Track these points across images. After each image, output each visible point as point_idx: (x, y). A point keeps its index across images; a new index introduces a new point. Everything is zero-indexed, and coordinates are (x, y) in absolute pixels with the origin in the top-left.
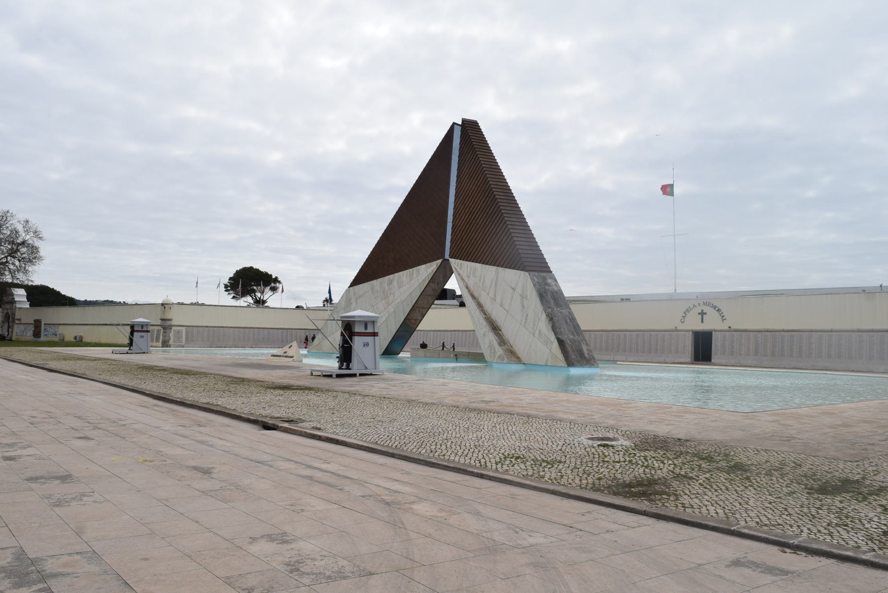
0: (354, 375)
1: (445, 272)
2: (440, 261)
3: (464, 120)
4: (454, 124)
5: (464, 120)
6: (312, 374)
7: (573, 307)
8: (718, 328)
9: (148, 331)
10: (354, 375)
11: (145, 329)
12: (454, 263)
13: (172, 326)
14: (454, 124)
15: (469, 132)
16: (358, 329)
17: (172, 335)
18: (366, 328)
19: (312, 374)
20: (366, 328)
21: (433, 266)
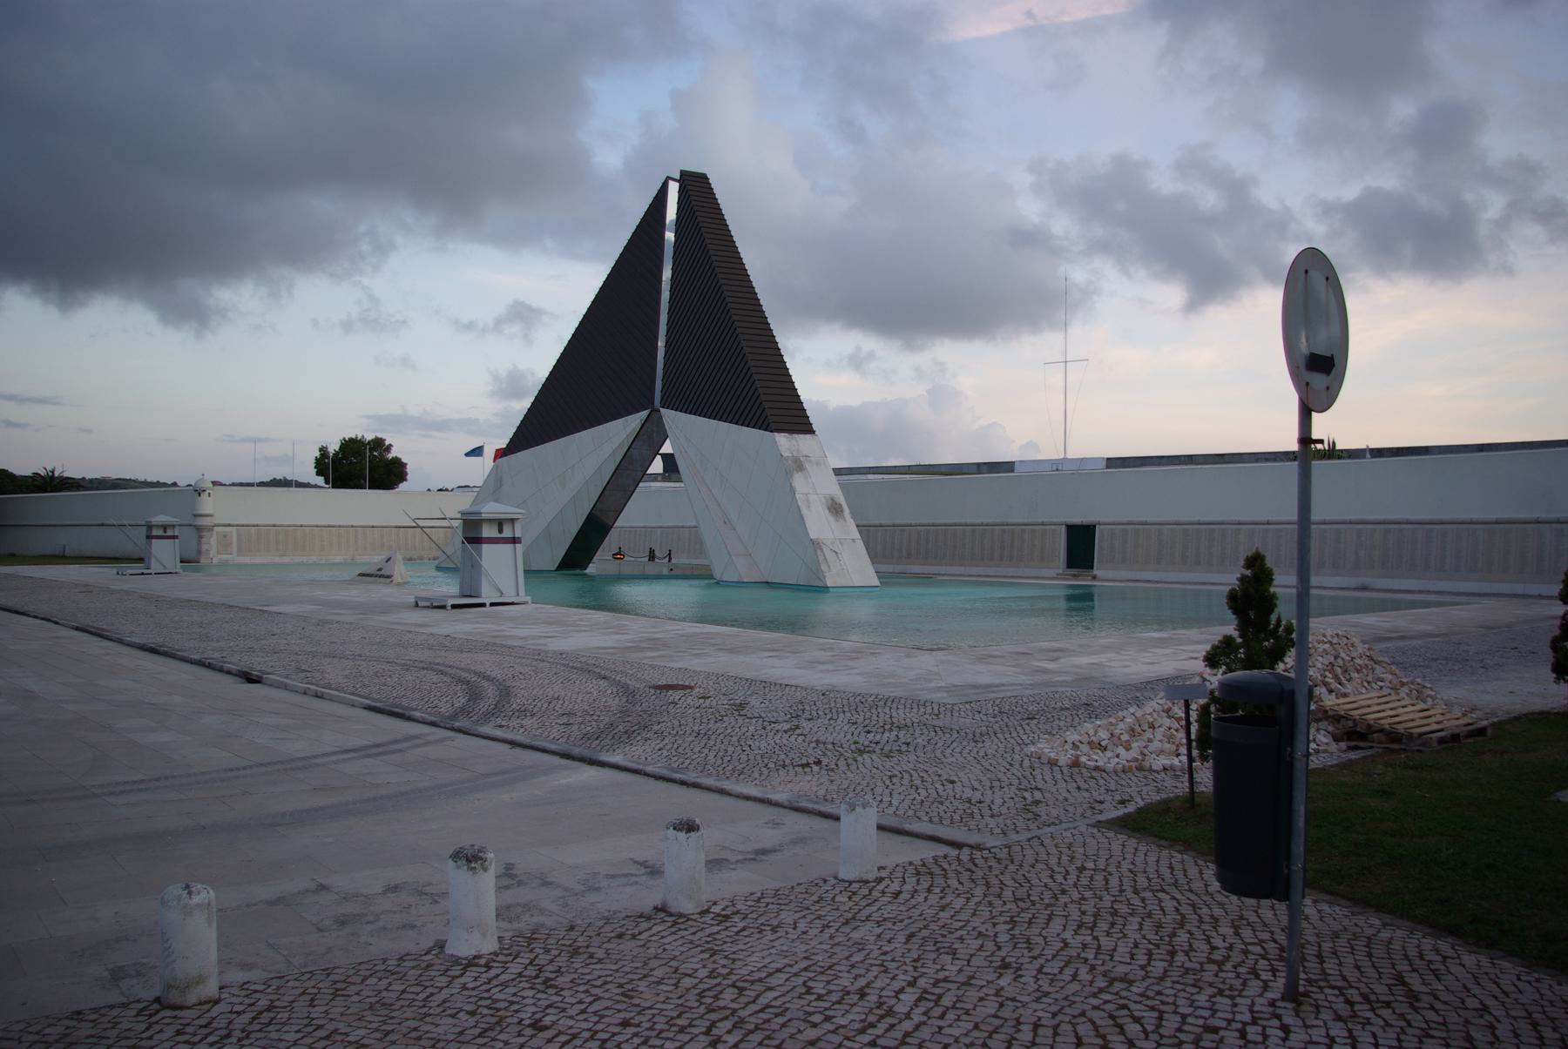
0: (483, 605)
1: (651, 436)
2: (644, 414)
3: (683, 173)
4: (668, 178)
5: (683, 173)
6: (417, 605)
7: (207, 505)
8: (1103, 519)
9: (174, 537)
10: (483, 605)
11: (169, 533)
12: (673, 419)
13: (210, 529)
14: (668, 178)
15: (696, 187)
16: (488, 532)
17: (213, 541)
18: (501, 531)
19: (417, 605)
20: (501, 531)
21: (635, 421)
